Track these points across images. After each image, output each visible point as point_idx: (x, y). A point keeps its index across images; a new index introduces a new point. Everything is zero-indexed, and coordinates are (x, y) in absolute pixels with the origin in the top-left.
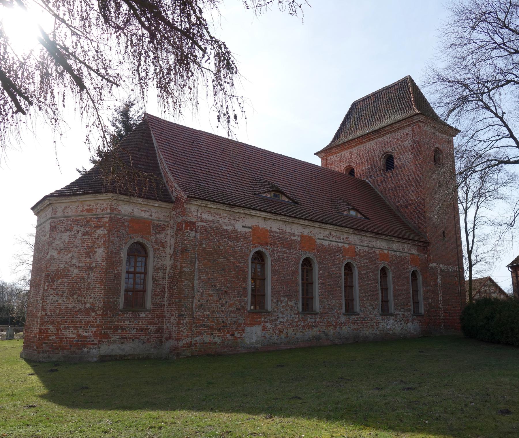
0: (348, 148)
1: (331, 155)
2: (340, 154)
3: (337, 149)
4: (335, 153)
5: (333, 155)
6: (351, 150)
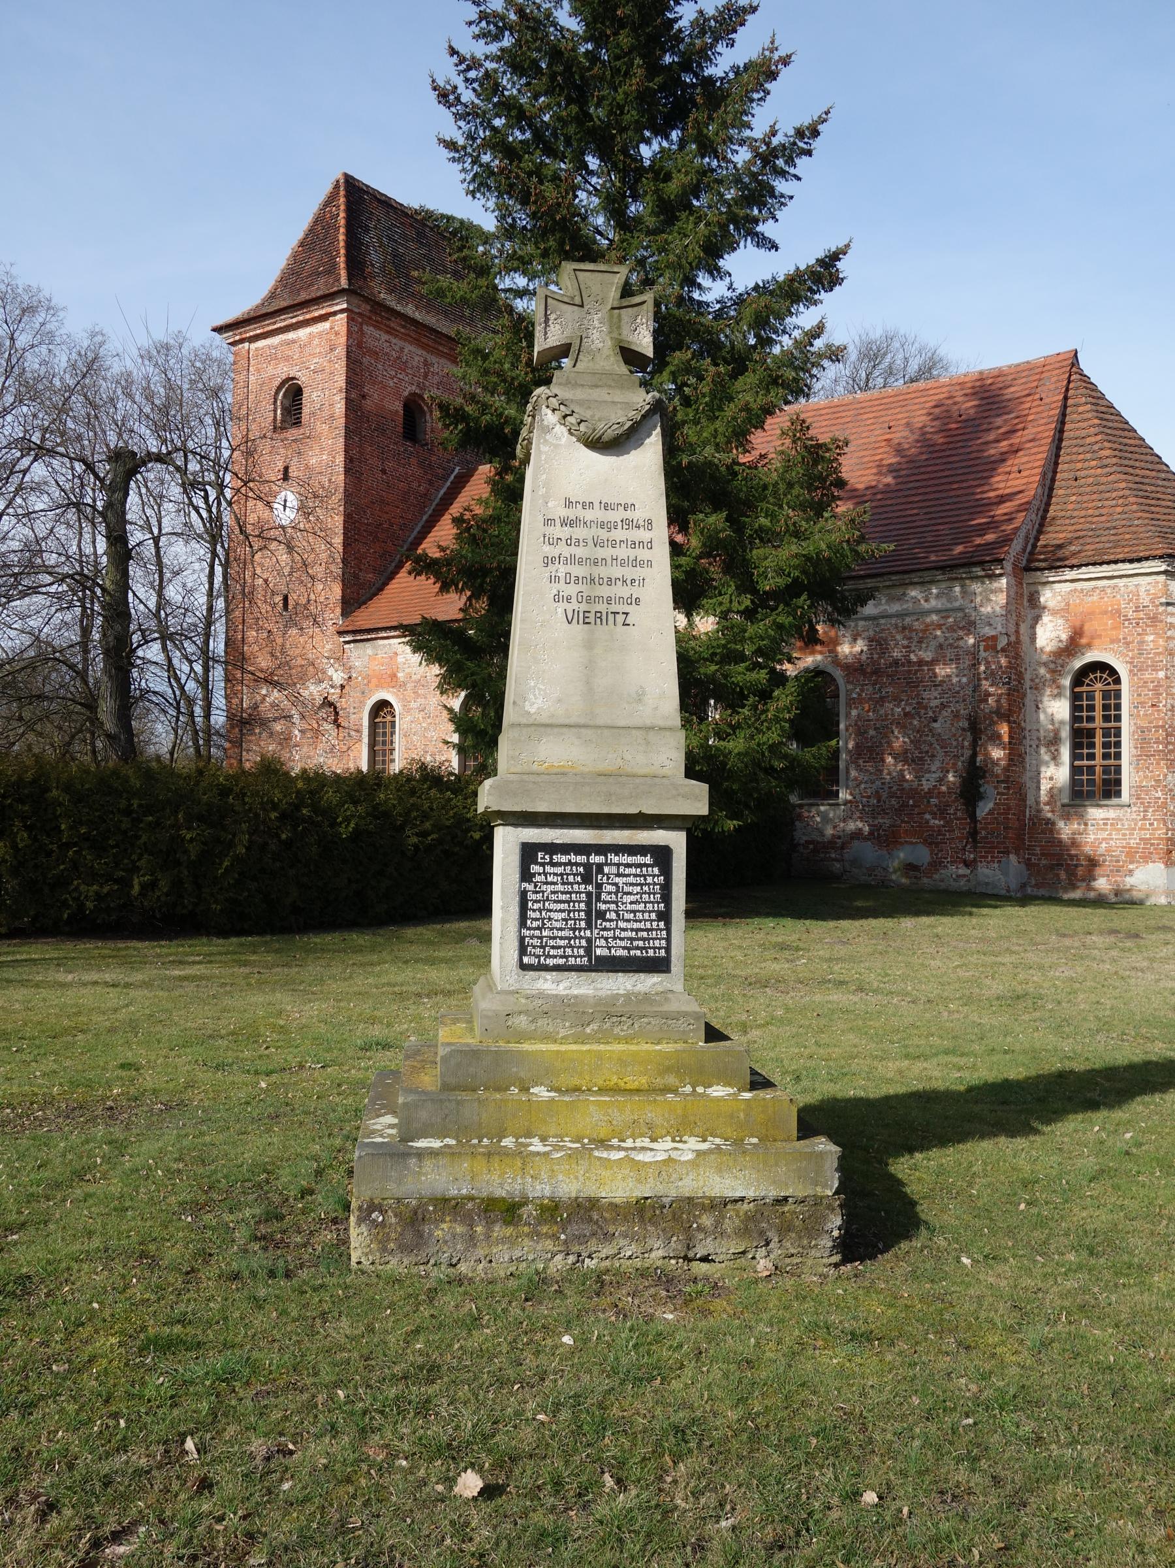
0: (424, 347)
1: (375, 327)
2: (400, 343)
3: (403, 327)
4: (390, 331)
5: (380, 329)
6: (432, 359)
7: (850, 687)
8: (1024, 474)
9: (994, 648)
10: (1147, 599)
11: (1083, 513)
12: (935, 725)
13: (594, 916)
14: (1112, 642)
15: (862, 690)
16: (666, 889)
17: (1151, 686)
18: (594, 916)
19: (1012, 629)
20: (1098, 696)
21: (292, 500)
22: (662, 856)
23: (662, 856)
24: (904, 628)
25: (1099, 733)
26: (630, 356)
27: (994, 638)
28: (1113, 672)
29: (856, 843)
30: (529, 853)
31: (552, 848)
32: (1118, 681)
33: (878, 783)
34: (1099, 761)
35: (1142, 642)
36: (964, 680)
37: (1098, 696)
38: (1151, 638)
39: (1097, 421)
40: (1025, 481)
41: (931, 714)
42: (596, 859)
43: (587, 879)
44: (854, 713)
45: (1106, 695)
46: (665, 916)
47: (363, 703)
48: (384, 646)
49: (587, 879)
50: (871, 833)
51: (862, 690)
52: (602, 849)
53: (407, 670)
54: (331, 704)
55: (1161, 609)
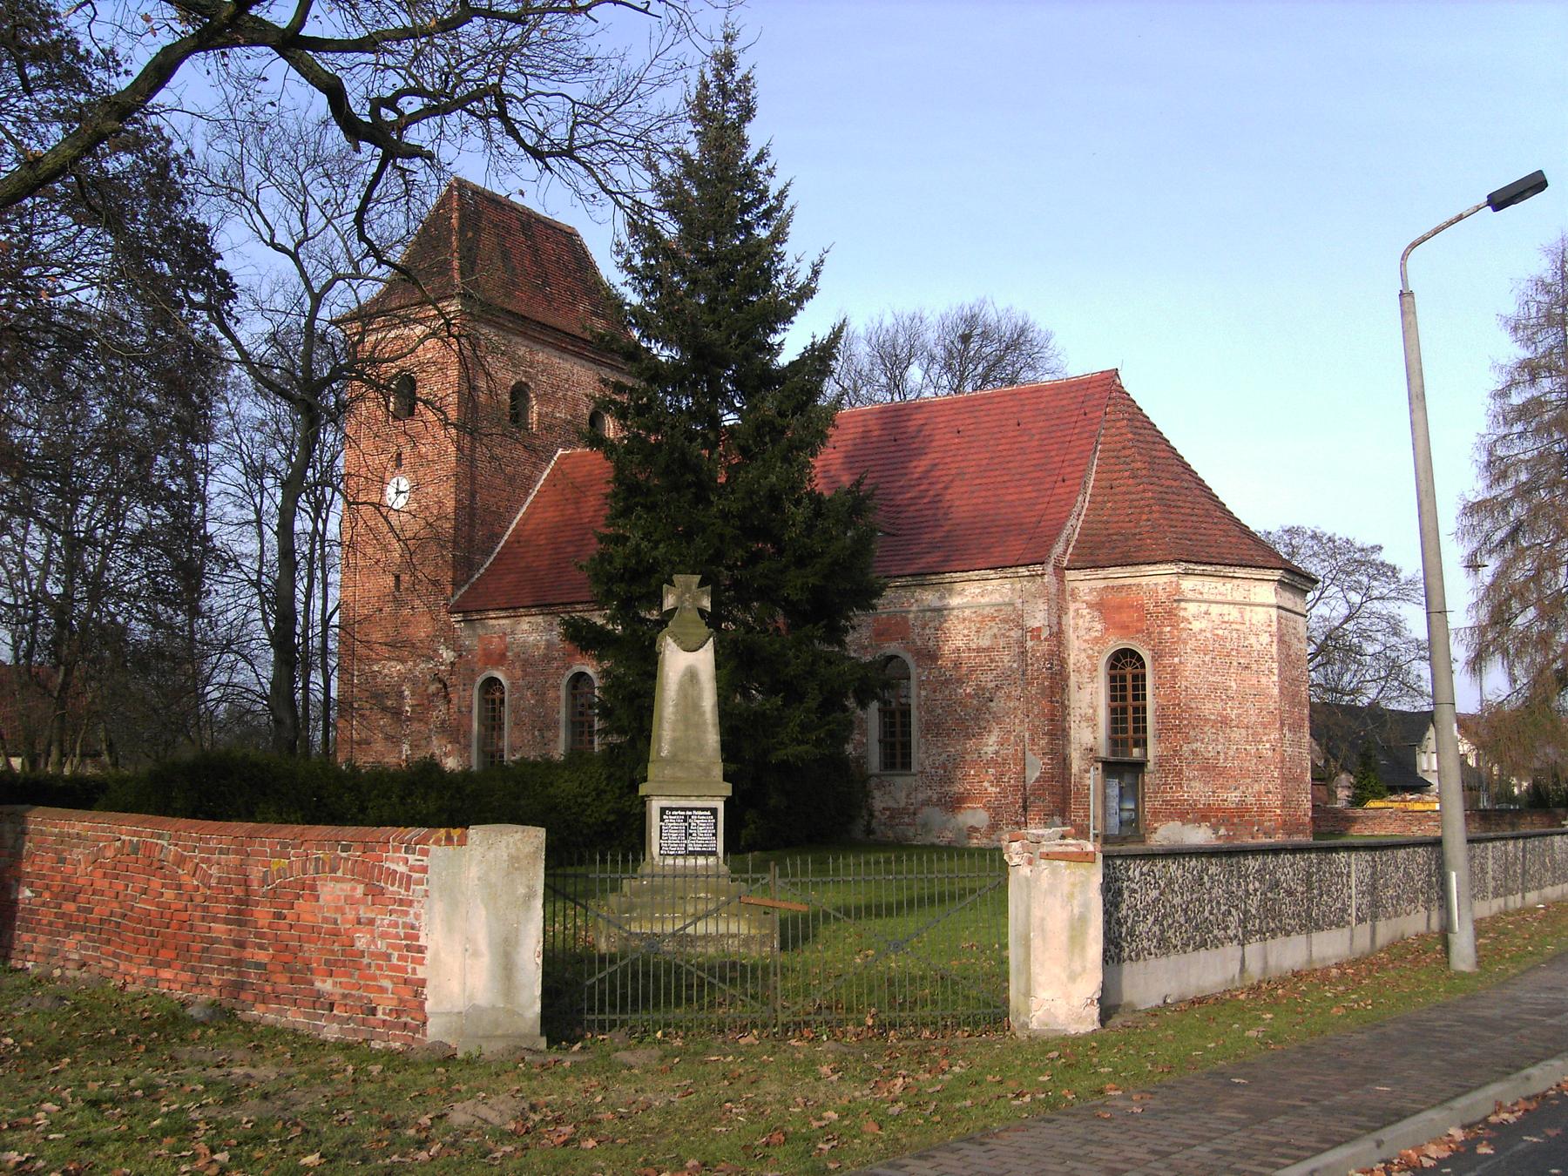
7: (920, 670)
8: (1067, 483)
9: (1039, 637)
10: (1165, 596)
11: (1116, 519)
12: (991, 704)
13: (688, 835)
14: (1138, 632)
15: (930, 673)
16: (715, 825)
17: (1169, 670)
18: (688, 835)
19: (1054, 620)
20: (1129, 678)
21: (405, 484)
22: (714, 811)
23: (714, 811)
24: (964, 620)
25: (1130, 710)
26: (701, 612)
27: (1039, 629)
28: (1140, 658)
29: (926, 810)
30: (663, 811)
31: (672, 809)
32: (1143, 666)
33: (944, 755)
34: (1131, 733)
35: (1161, 633)
36: (1015, 665)
37: (1129, 678)
38: (1168, 629)
39: (1130, 436)
40: (1068, 490)
41: (987, 695)
42: (689, 813)
43: (685, 821)
44: (923, 693)
45: (1135, 678)
46: (715, 835)
47: (473, 681)
48: (493, 626)
49: (685, 821)
50: (939, 800)
51: (930, 673)
52: (691, 809)
53: (516, 650)
54: (440, 681)
55: (1175, 605)
